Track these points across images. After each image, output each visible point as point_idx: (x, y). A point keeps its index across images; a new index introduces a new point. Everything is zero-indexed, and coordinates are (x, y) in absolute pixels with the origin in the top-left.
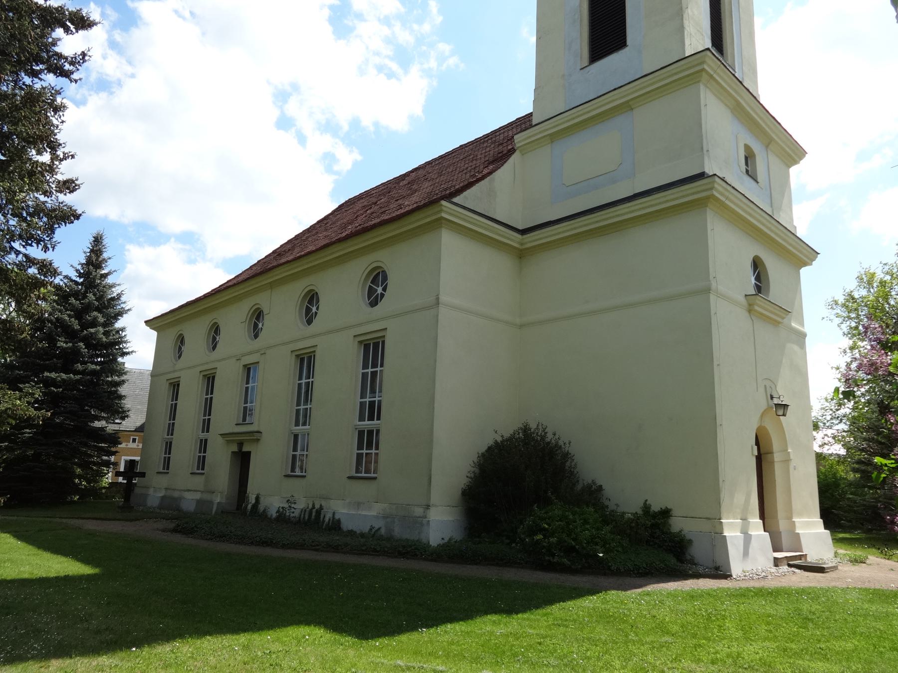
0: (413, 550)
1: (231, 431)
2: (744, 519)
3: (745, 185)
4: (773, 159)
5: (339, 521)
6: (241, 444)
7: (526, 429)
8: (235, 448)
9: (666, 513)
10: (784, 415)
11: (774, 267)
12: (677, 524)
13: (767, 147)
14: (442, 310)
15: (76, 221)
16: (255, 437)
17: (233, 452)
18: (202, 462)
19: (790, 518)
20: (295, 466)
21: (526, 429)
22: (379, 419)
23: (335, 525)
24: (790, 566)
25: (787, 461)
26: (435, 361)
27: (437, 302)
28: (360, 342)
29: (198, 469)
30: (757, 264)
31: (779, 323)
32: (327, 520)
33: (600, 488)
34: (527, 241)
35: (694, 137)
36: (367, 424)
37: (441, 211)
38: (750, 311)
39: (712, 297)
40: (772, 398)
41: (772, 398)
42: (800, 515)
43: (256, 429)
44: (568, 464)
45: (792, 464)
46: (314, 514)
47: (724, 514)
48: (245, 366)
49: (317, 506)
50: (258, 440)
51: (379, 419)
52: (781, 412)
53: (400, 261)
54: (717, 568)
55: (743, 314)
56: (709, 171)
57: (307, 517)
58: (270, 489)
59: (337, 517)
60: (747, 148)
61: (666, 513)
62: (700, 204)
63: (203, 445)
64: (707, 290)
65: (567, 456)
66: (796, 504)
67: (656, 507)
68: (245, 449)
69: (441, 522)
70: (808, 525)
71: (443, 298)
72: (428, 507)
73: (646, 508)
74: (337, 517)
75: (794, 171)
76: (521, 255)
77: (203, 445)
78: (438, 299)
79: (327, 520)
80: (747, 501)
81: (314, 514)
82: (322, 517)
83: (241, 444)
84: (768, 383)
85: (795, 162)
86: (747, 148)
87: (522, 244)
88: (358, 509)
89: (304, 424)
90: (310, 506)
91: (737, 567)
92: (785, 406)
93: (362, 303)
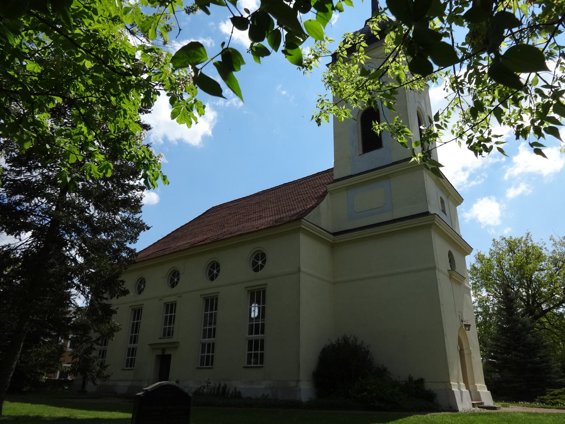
0: (295, 405)
1: (156, 342)
2: (458, 383)
3: (442, 215)
4: (450, 203)
5: (239, 392)
6: (164, 350)
7: (345, 339)
8: (159, 352)
9: (421, 381)
10: (469, 330)
11: (455, 254)
12: (428, 386)
13: (448, 197)
14: (302, 275)
15: (147, 231)
16: (175, 346)
17: (157, 355)
18: (130, 363)
19: (474, 384)
20: (207, 361)
21: (345, 339)
22: (214, 337)
23: (237, 395)
24: (479, 407)
25: (470, 354)
26: (299, 302)
27: (299, 270)
28: (248, 291)
29: (127, 366)
30: (450, 254)
31: (461, 283)
32: (231, 392)
33: (385, 369)
34: (338, 239)
35: (423, 196)
36: (132, 346)
37: (301, 224)
38: (450, 278)
39: (437, 272)
40: (462, 321)
41: (462, 321)
42: (478, 383)
43: (175, 341)
44: (369, 357)
45: (473, 355)
46: (221, 389)
47: (451, 380)
48: (165, 303)
49: (222, 385)
50: (177, 347)
51: (214, 337)
52: (467, 329)
53: (274, 250)
54: (451, 407)
55: (448, 280)
56: (432, 211)
57: (216, 392)
58: (187, 375)
59: (238, 390)
60: (441, 198)
61: (421, 381)
62: (428, 227)
63: (132, 352)
64: (434, 268)
65: (367, 352)
66: (476, 377)
67: (415, 378)
68: (167, 352)
69: (305, 390)
70: (481, 387)
71: (302, 269)
72: (298, 381)
73: (411, 378)
74: (238, 390)
75: (458, 208)
76: (333, 247)
77: (132, 352)
78: (299, 269)
79: (231, 392)
80: (458, 373)
81: (221, 389)
82: (227, 391)
83: (164, 350)
84: (460, 315)
85: (459, 204)
86: (441, 198)
87: (334, 241)
88: (250, 384)
89: (134, 343)
90: (218, 385)
91: (460, 407)
92: (469, 325)
93: (250, 270)
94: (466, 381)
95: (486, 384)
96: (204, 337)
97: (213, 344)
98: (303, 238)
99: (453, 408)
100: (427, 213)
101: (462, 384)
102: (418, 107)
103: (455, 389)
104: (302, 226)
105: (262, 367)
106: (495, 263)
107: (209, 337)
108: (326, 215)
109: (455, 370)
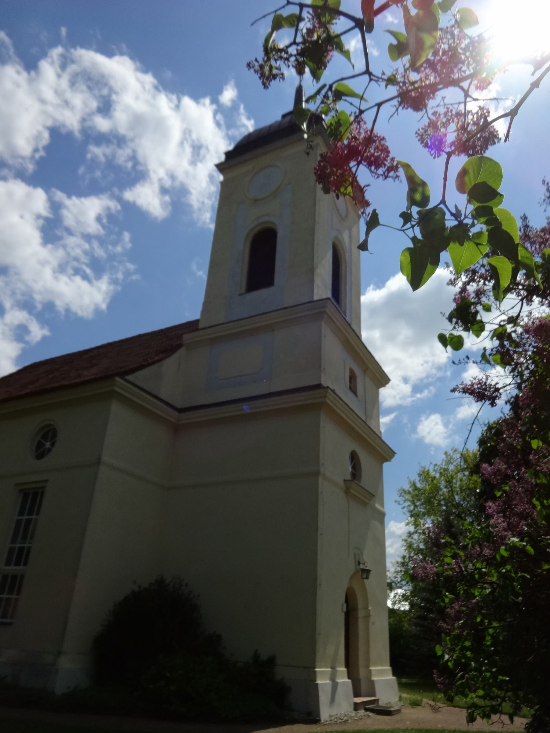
2: (333, 668)
9: (271, 662)
12: (281, 673)
19: (368, 666)
24: (366, 710)
27: (99, 462)
28: (20, 491)
34: (183, 419)
38: (347, 491)
40: (359, 563)
41: (359, 563)
42: (376, 665)
45: (372, 619)
60: (351, 371)
61: (271, 662)
62: (319, 406)
64: (317, 474)
66: (373, 656)
69: (69, 669)
70: (381, 672)
71: (105, 458)
73: (256, 657)
76: (176, 429)
86: (351, 371)
91: (325, 713)
92: (368, 571)
94: (350, 663)
95: (391, 665)
96: (8, 563)
97: (22, 577)
98: (116, 408)
99: (312, 717)
100: (319, 386)
101: (342, 669)
102: (336, 238)
103: (323, 681)
104: (116, 389)
105: (10, 624)
106: (442, 484)
107: (17, 563)
108: (170, 378)
109: (332, 644)
